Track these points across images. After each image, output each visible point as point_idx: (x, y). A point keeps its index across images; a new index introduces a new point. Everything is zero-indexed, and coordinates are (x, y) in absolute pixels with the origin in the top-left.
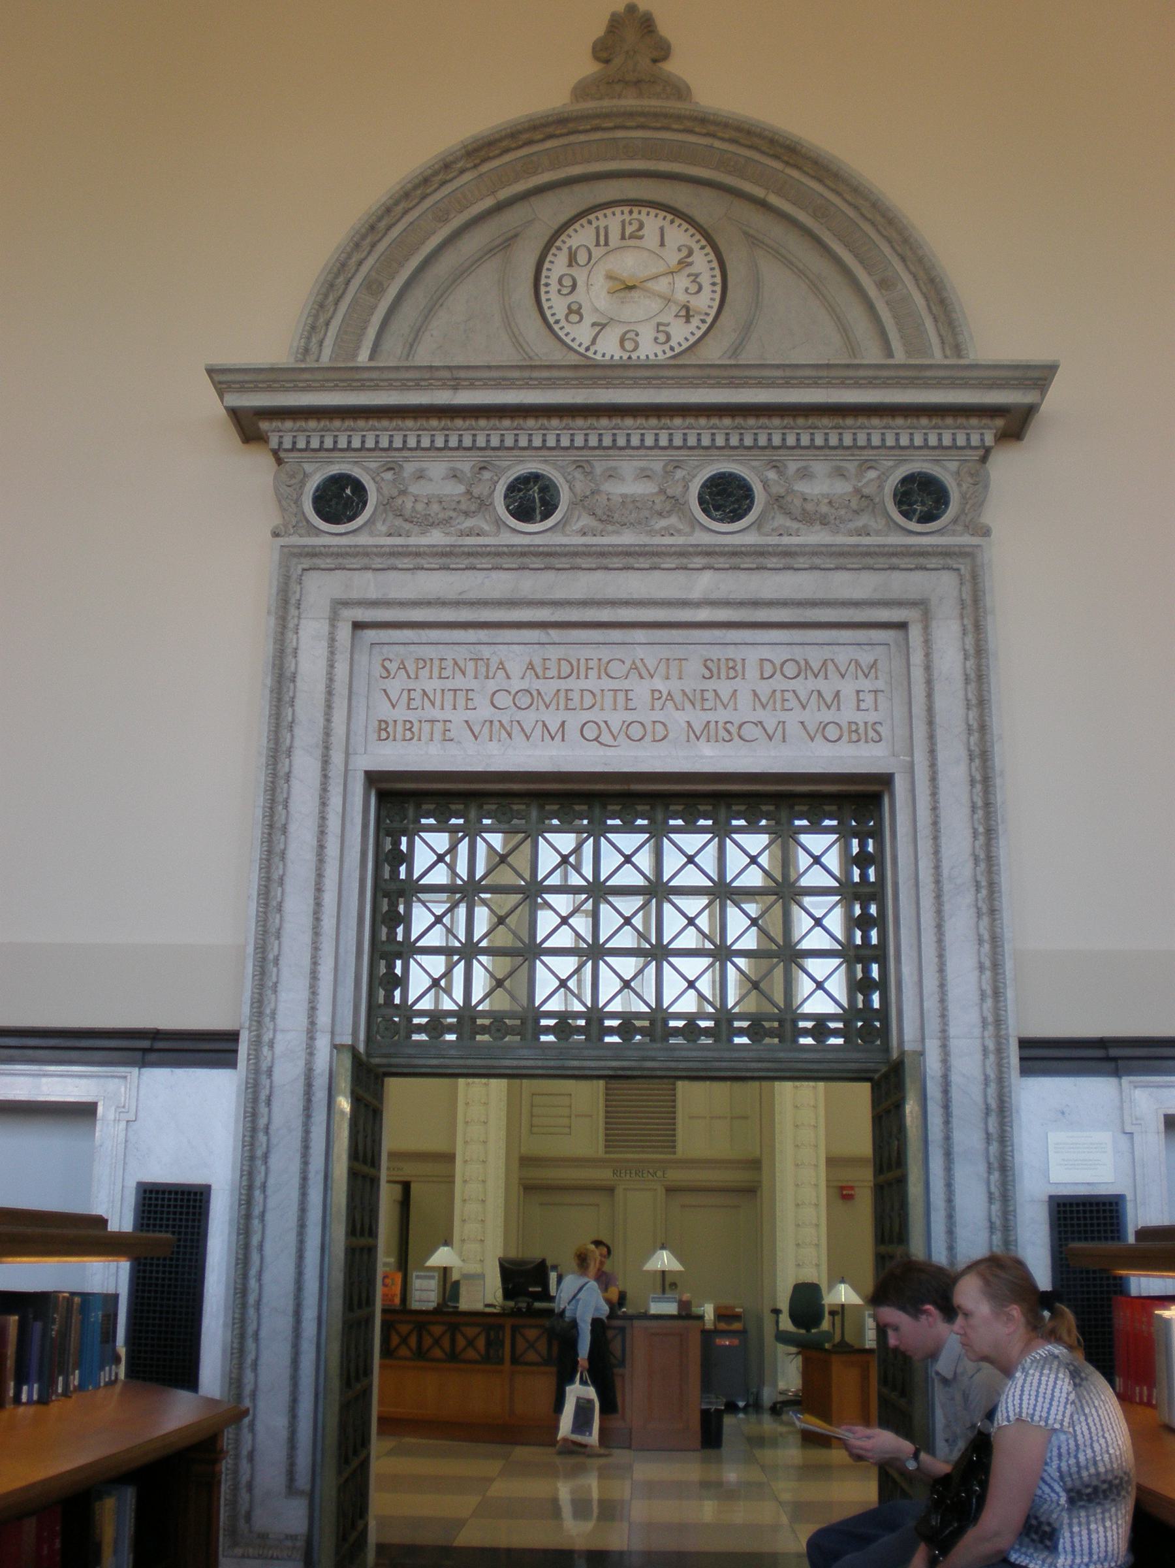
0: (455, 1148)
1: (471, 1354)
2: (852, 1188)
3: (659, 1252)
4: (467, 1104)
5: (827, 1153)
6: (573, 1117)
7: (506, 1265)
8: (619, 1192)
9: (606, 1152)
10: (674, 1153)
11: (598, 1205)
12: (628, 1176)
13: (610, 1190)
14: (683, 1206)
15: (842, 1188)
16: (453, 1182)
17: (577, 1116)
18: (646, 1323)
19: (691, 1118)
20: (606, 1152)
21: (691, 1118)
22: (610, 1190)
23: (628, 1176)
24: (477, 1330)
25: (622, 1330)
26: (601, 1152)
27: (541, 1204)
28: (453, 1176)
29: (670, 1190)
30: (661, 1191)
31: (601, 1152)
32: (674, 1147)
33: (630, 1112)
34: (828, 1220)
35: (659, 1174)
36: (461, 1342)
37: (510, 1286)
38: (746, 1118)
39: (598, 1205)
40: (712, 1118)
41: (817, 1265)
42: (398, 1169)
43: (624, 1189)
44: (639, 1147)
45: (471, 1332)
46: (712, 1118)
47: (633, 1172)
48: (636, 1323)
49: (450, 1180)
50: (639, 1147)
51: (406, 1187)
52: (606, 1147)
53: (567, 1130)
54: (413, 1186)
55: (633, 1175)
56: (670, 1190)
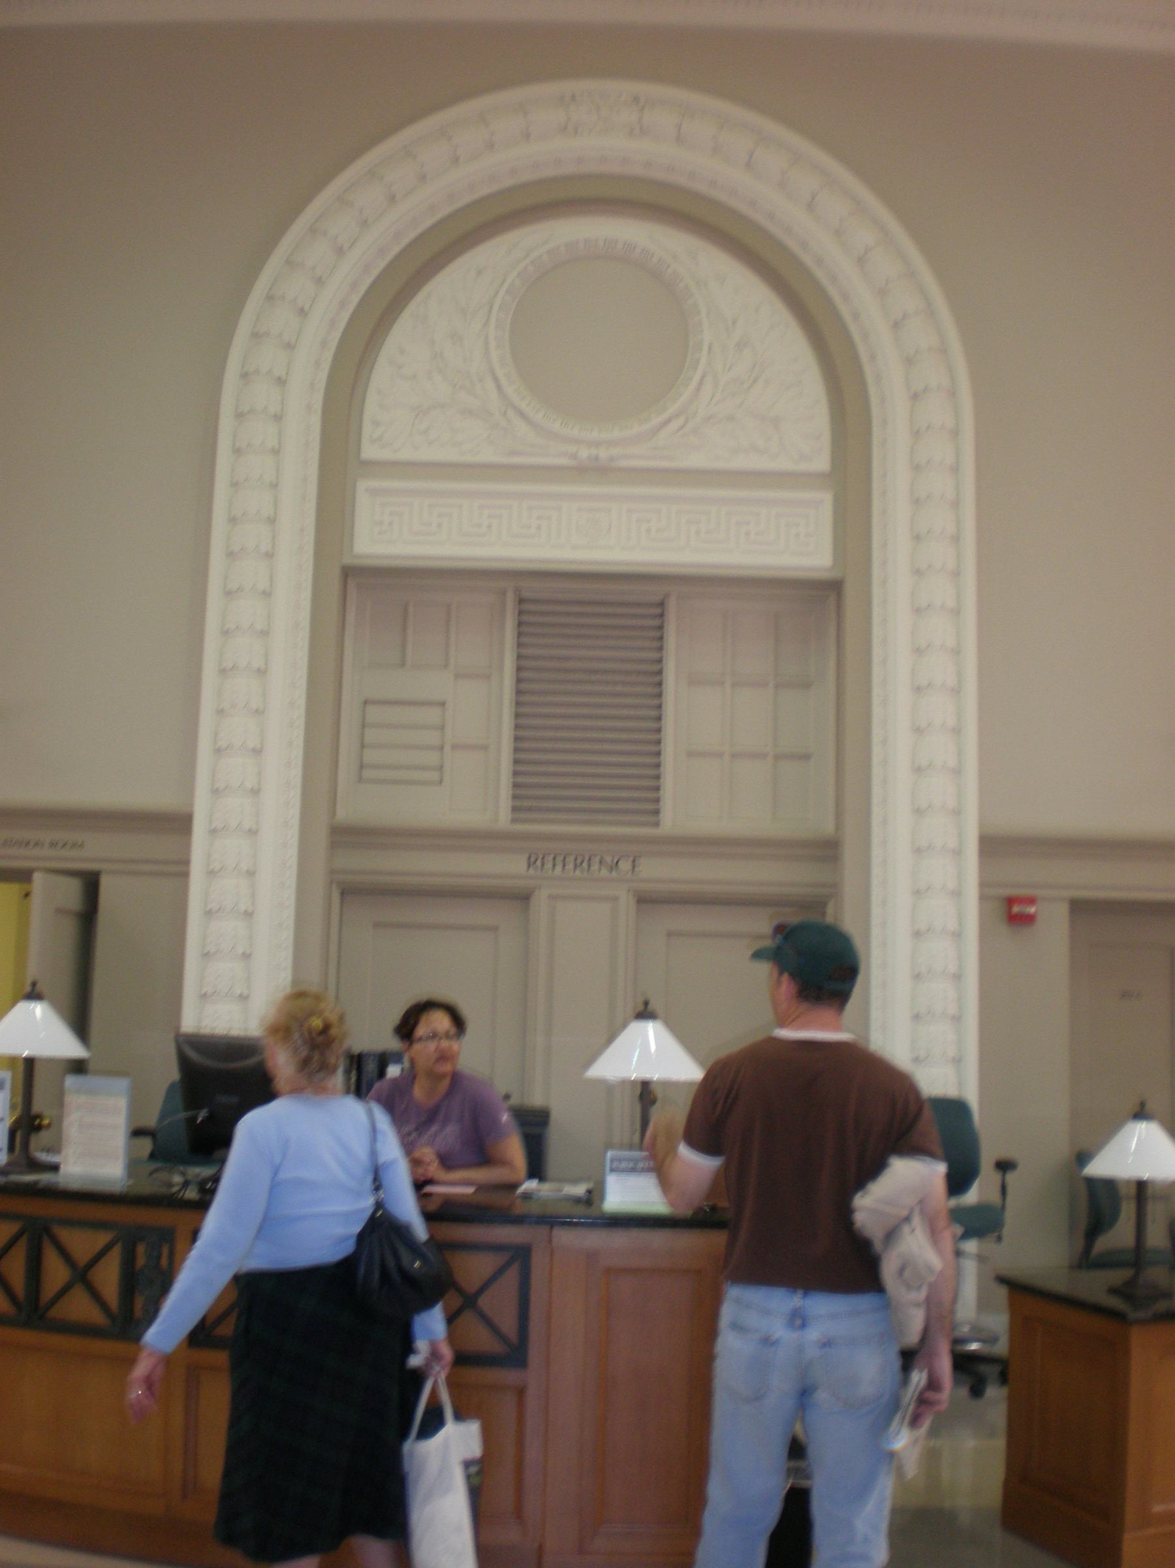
0: (191, 805)
1: (79, 1307)
2: (1031, 901)
3: (636, 1027)
4: (220, 712)
5: (982, 824)
6: (447, 749)
7: (192, 1055)
8: (541, 901)
9: (514, 821)
10: (657, 824)
11: (495, 929)
12: (559, 868)
13: (522, 898)
14: (670, 934)
15: (1010, 901)
16: (185, 875)
17: (455, 747)
18: (596, 1239)
19: (691, 754)
20: (514, 821)
21: (691, 754)
22: (522, 898)
23: (559, 868)
24: (102, 1239)
25: (521, 1255)
26: (502, 817)
27: (376, 925)
28: (187, 862)
29: (646, 901)
30: (626, 902)
31: (502, 817)
32: (657, 812)
33: (568, 614)
34: (12, 1086)
35: (625, 866)
36: (56, 1272)
37: (202, 1115)
38: (806, 757)
39: (495, 929)
40: (734, 756)
41: (957, 1061)
42: (74, 845)
43: (550, 897)
44: (585, 810)
45: (83, 1243)
46: (734, 756)
47: (571, 859)
48: (565, 1237)
49: (180, 870)
50: (585, 810)
51: (91, 884)
52: (515, 809)
53: (435, 776)
54: (105, 883)
55: (570, 866)
56: (646, 901)
